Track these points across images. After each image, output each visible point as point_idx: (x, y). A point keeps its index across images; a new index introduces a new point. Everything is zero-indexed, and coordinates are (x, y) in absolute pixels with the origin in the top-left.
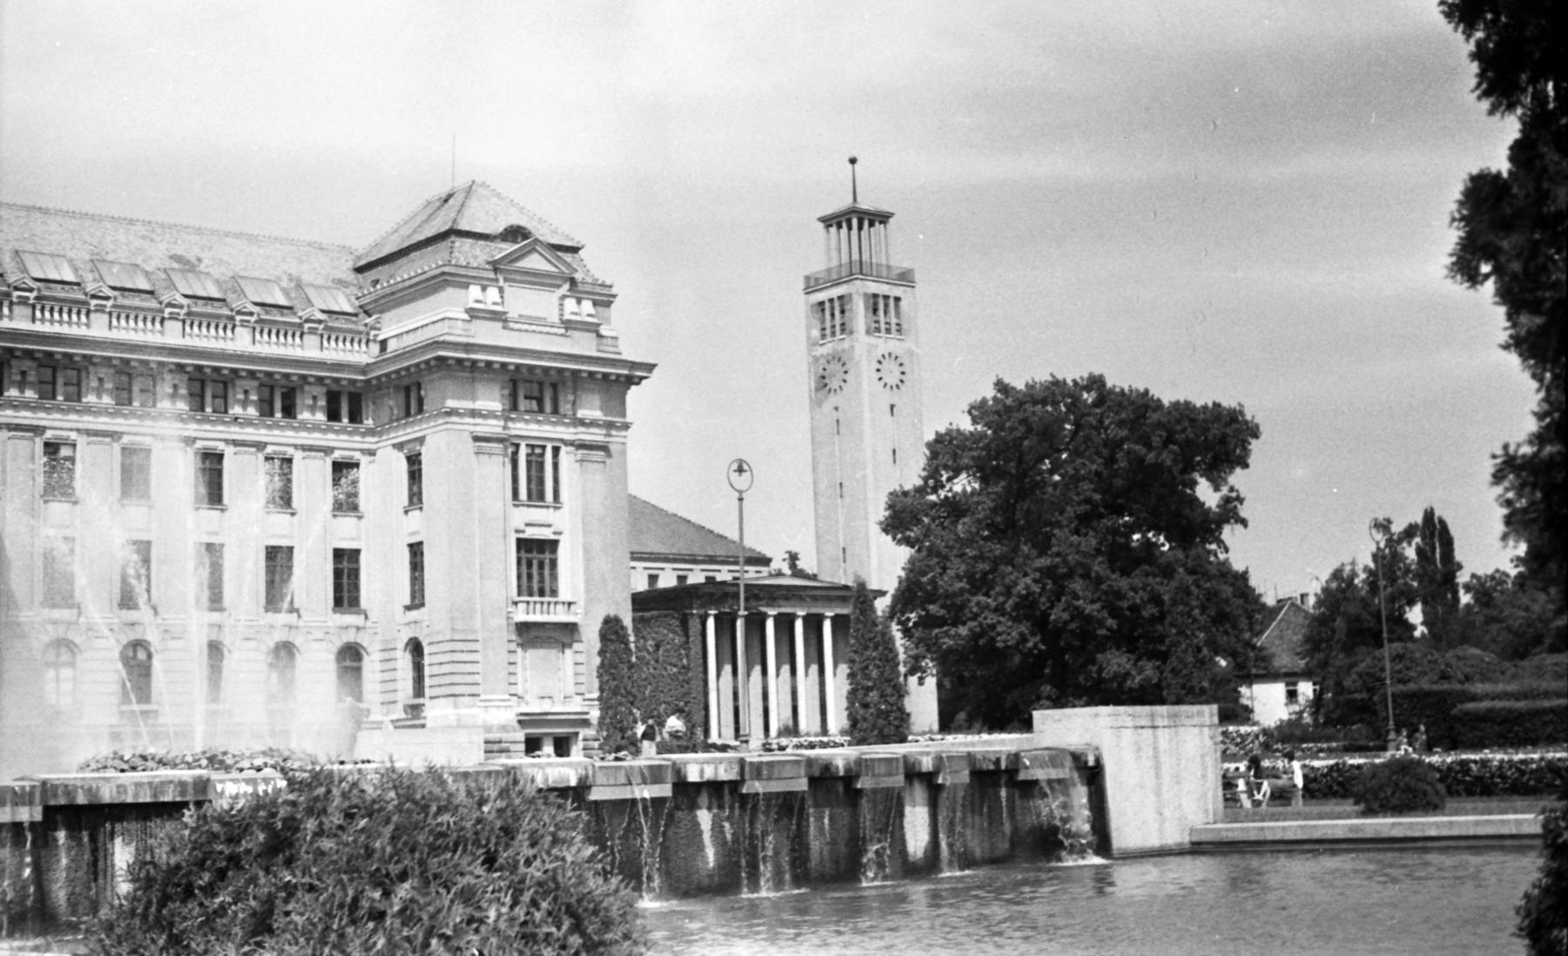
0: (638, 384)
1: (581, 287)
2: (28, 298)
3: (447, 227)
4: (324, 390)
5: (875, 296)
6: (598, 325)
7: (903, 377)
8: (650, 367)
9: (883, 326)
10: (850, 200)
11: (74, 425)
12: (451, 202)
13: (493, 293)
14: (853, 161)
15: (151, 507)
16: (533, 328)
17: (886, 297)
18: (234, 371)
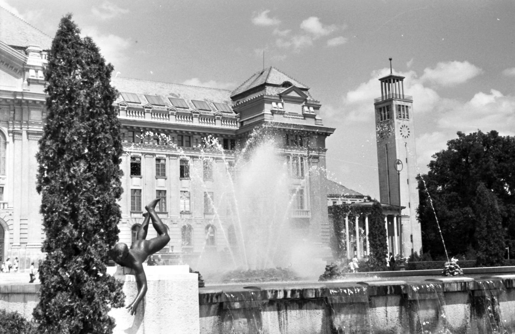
0: (329, 135)
1: (308, 102)
2: (124, 108)
3: (264, 82)
4: (222, 139)
5: (399, 106)
6: (315, 115)
7: (409, 133)
8: (333, 130)
9: (402, 116)
10: (390, 73)
11: (140, 151)
12: (263, 74)
13: (280, 105)
14: (390, 59)
15: (166, 179)
16: (296, 117)
17: (403, 106)
18: (193, 133)
